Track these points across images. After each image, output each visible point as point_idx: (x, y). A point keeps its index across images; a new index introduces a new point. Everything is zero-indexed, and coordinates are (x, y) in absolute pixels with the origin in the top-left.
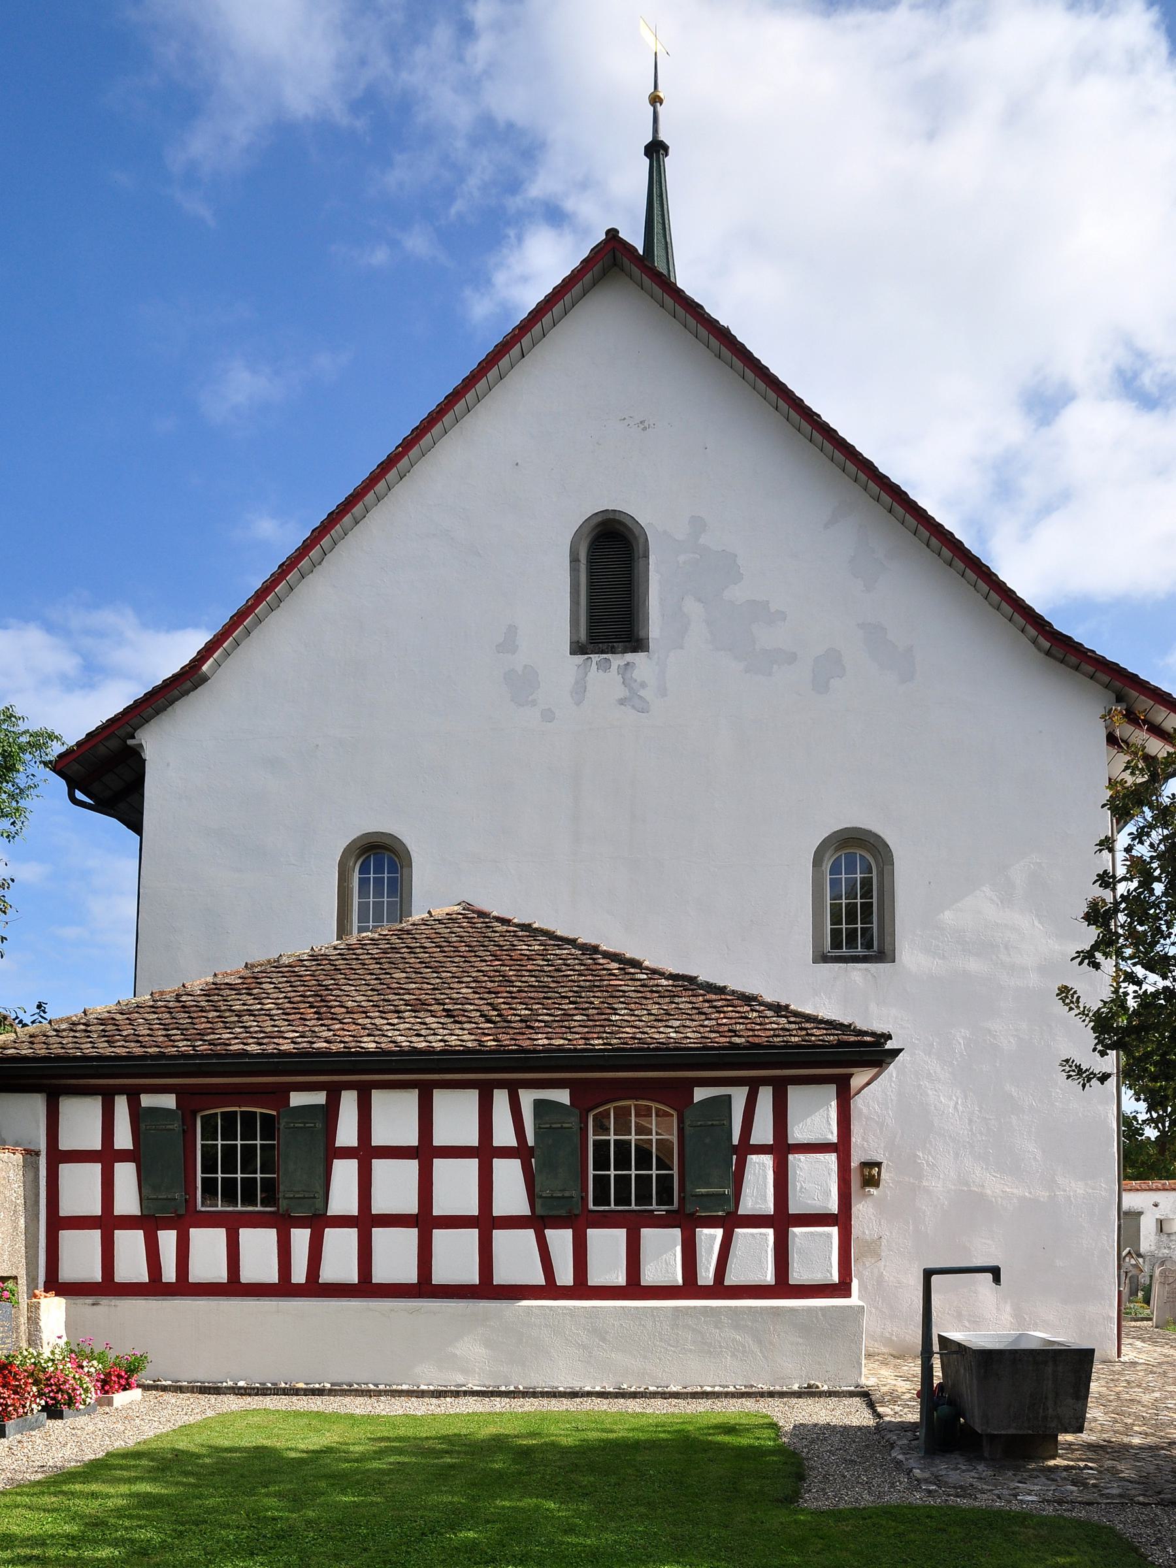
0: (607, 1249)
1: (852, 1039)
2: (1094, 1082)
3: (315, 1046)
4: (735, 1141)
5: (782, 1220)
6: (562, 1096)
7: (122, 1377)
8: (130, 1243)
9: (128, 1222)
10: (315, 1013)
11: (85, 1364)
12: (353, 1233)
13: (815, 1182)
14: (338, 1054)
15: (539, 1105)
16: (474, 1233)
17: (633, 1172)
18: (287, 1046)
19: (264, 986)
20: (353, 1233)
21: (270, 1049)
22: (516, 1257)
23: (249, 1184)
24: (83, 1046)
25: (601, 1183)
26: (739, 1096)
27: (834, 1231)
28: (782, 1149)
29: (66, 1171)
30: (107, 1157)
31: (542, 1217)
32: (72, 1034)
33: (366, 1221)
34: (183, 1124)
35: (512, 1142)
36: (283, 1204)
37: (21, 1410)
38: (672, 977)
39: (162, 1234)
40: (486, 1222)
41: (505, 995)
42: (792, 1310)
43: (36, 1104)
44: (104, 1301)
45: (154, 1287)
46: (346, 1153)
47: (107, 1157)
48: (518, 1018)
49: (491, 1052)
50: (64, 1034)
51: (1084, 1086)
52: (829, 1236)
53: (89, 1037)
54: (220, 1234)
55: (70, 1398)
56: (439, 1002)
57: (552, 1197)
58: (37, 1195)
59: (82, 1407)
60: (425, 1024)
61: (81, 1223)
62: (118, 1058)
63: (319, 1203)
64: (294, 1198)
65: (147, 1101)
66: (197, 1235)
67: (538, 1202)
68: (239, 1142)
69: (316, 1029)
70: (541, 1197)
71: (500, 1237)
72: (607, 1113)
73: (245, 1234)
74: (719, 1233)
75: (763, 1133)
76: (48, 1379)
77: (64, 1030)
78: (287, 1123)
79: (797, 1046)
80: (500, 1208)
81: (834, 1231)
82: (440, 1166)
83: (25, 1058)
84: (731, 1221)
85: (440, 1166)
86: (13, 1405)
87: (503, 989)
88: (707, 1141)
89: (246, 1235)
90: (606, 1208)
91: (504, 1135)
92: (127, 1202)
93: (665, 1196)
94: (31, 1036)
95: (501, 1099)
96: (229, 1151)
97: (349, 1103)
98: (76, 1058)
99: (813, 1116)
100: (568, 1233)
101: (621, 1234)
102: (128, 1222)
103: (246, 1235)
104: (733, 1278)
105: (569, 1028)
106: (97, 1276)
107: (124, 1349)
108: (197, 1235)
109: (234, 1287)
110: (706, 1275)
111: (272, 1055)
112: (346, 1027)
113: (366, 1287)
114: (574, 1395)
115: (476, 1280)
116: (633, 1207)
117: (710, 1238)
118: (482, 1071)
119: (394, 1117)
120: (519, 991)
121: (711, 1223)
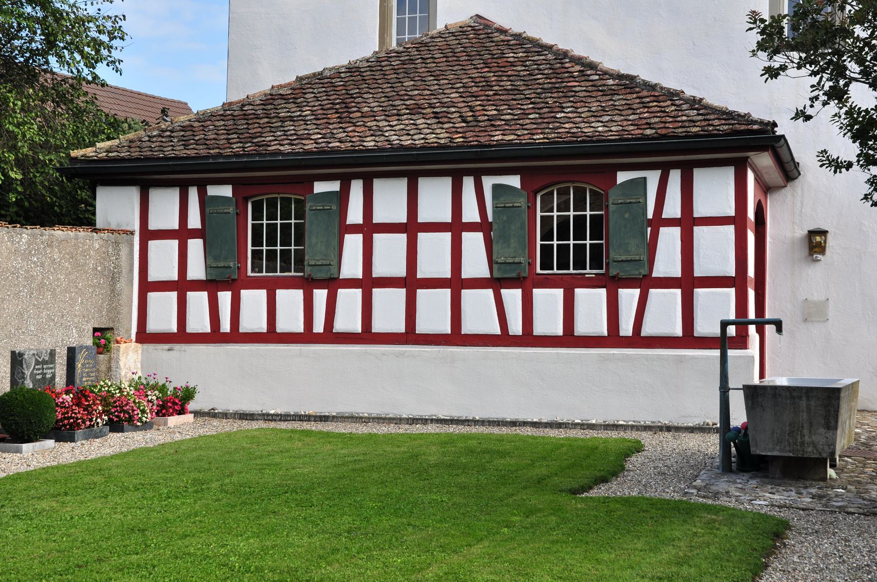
0: (548, 303)
1: (743, 127)
2: (843, 170)
3: (330, 145)
4: (650, 215)
5: (688, 282)
6: (514, 181)
7: (177, 404)
8: (198, 301)
9: (197, 285)
10: (338, 117)
11: (149, 393)
12: (358, 293)
13: (716, 251)
14: (346, 151)
15: (496, 188)
16: (403, 292)
17: (572, 242)
18: (310, 146)
19: (306, 96)
20: (358, 293)
21: (297, 149)
22: (480, 311)
23: (285, 254)
24: (165, 149)
25: (546, 251)
26: (653, 178)
27: (732, 291)
28: (688, 222)
29: (154, 245)
30: (182, 234)
31: (499, 279)
32: (160, 139)
33: (368, 283)
34: (237, 208)
35: (477, 219)
36: (308, 269)
37: (88, 423)
38: (621, 77)
39: (221, 295)
40: (456, 284)
41: (483, 98)
42: (693, 358)
43: (132, 194)
44: (177, 347)
45: (215, 336)
46: (354, 229)
47: (182, 234)
48: (486, 118)
49: (458, 147)
50: (154, 139)
51: (835, 172)
52: (728, 295)
53: (172, 141)
54: (262, 294)
55: (130, 417)
56: (431, 106)
57: (505, 263)
58: (132, 265)
59: (139, 424)
60: (416, 125)
61: (163, 286)
62: (189, 158)
63: (334, 270)
64: (315, 265)
65: (213, 191)
66: (246, 294)
67: (495, 266)
68: (279, 222)
69: (335, 131)
70: (497, 263)
71: (467, 294)
72: (552, 193)
73: (280, 294)
74: (637, 292)
75: (673, 208)
76: (115, 402)
77: (155, 136)
78: (311, 206)
79: (696, 135)
80: (467, 273)
81: (732, 291)
82: (423, 238)
83: (123, 160)
84: (647, 282)
85: (423, 238)
86: (81, 418)
87: (483, 93)
88: (627, 216)
89: (281, 294)
90: (550, 272)
91: (471, 213)
92: (197, 270)
93: (596, 263)
94: (130, 142)
95: (468, 184)
96: (272, 228)
97: (357, 189)
98: (159, 159)
99: (715, 191)
100: (518, 293)
101: (559, 293)
102: (197, 285)
103: (281, 294)
104: (649, 329)
105: (522, 125)
106: (174, 328)
107: (177, 382)
108: (246, 294)
109: (272, 335)
110: (626, 328)
111: (298, 154)
112: (357, 129)
113: (367, 336)
114: (514, 423)
115: (448, 331)
116: (572, 271)
117: (629, 297)
118: (457, 163)
119: (390, 199)
120: (494, 94)
121: (629, 283)
